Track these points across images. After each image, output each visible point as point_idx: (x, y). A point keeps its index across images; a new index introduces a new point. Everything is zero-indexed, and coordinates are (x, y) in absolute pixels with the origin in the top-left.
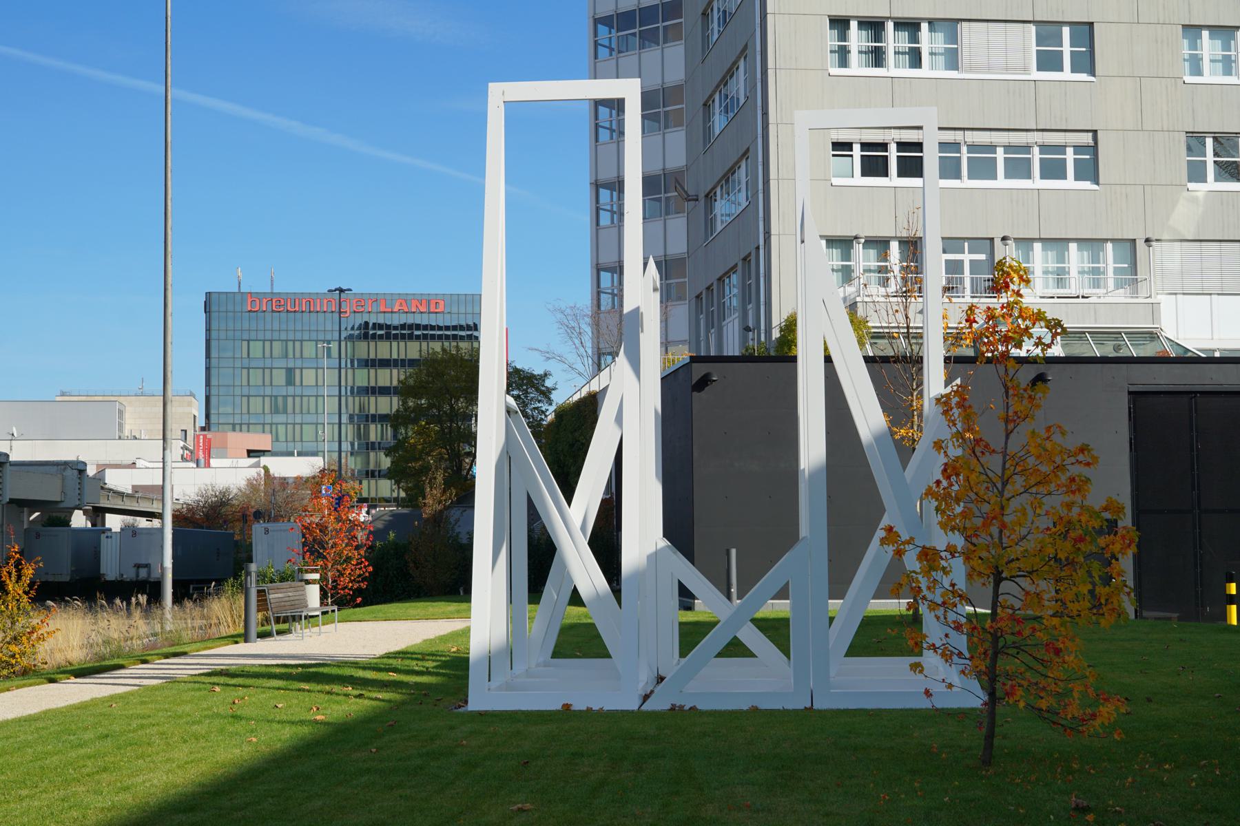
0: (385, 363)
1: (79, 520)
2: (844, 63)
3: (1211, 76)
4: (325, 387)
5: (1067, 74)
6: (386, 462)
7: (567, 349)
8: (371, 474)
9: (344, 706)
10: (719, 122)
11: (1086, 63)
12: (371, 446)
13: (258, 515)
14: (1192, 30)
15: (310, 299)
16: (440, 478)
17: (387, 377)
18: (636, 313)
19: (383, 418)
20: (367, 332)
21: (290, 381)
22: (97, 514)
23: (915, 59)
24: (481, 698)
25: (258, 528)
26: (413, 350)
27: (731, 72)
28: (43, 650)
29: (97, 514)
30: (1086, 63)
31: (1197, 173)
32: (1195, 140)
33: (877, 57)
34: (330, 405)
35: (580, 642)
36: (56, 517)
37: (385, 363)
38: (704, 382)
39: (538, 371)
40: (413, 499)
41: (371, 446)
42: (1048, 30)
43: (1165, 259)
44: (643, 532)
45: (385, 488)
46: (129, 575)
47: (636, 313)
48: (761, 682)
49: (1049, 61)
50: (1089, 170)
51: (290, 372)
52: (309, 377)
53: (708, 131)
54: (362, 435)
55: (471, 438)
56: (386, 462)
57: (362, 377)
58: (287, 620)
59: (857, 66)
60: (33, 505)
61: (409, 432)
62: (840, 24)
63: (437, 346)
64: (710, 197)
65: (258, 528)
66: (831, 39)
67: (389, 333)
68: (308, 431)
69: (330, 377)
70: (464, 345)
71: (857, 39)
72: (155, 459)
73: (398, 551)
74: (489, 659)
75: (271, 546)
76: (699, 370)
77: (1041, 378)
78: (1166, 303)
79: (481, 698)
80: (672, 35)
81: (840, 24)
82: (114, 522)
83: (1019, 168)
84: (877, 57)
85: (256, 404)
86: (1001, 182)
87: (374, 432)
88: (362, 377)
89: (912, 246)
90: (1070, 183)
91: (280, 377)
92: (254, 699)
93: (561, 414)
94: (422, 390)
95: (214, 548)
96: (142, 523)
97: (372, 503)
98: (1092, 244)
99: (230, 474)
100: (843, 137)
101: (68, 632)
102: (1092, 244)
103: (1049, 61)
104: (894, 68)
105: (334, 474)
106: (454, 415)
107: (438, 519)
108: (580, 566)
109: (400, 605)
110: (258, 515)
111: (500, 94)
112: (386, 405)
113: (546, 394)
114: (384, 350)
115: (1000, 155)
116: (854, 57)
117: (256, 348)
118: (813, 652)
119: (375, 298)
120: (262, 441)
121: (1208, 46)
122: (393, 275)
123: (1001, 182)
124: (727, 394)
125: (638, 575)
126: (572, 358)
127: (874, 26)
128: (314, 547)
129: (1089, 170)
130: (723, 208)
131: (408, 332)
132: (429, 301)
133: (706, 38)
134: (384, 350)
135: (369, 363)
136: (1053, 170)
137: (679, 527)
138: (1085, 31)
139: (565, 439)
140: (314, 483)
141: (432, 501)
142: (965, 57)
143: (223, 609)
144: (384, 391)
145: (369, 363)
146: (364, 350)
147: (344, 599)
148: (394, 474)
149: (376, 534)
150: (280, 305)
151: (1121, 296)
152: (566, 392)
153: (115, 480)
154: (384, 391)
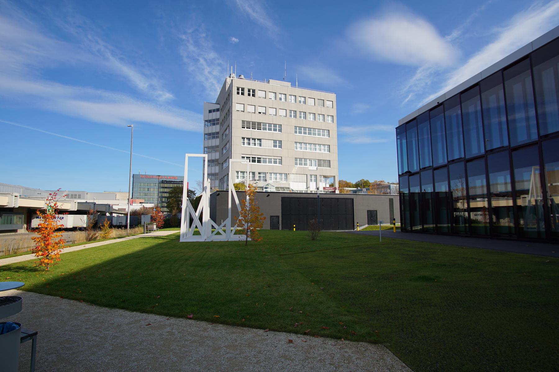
0: (166, 188)
1: (108, 214)
2: (244, 144)
3: (299, 150)
4: (155, 193)
5: (278, 148)
6: (166, 205)
7: (198, 188)
8: (163, 207)
9: (161, 241)
10: (224, 152)
11: (280, 147)
12: (163, 202)
13: (142, 214)
14: (296, 143)
15: (153, 176)
16: (176, 208)
17: (166, 190)
18: (206, 187)
19: (165, 197)
20: (163, 182)
21: (148, 190)
22: (111, 213)
23: (320, 150)
24: (182, 240)
25: (142, 216)
26: (171, 185)
27: (226, 144)
28: (111, 235)
29: (111, 213)
30: (280, 147)
31: (296, 164)
32: (296, 159)
33: (249, 144)
34: (156, 195)
35: (197, 233)
36: (103, 214)
37: (166, 188)
38: (218, 195)
39: (193, 190)
40: (171, 211)
41: (163, 202)
42: (275, 141)
43: (291, 177)
44: (206, 217)
45: (165, 209)
46: (118, 224)
47: (206, 187)
48: (222, 238)
49: (275, 146)
50: (281, 163)
51: (148, 189)
52: (152, 190)
53: (222, 153)
54: (161, 200)
55: (181, 201)
56: (166, 205)
57: (162, 190)
58: (151, 230)
59: (246, 145)
60: (98, 212)
61: (170, 200)
62: (243, 138)
63: (175, 185)
64: (222, 164)
65: (142, 216)
66: (242, 140)
67: (167, 182)
68: (151, 199)
69: (156, 190)
70: (180, 185)
71: (246, 141)
72: (122, 204)
73: (168, 220)
74: (183, 235)
75: (145, 219)
76: (218, 193)
77: (268, 195)
78: (291, 183)
79: (182, 240)
80: (217, 137)
81: (243, 138)
82: (114, 215)
83: (270, 162)
84: (249, 144)
85: (142, 194)
86: (267, 164)
87: (164, 199)
88: (162, 190)
89: (254, 173)
90: (278, 164)
91: (146, 189)
92: (148, 241)
93: (196, 198)
94: (172, 193)
95: (136, 220)
96: (120, 215)
97: (163, 212)
98: (281, 174)
99: (136, 207)
100: (243, 156)
101: (114, 232)
102: (281, 174)
103: (275, 146)
104: (252, 146)
105: (157, 207)
106: (178, 197)
107: (175, 215)
108: (196, 222)
109: (98, 262)
110: (142, 214)
111: (187, 155)
112: (166, 195)
113: (195, 194)
114: (166, 185)
115: (267, 160)
116: (245, 144)
117: (142, 184)
118: (229, 233)
119: (165, 176)
120: (143, 201)
121: (298, 145)
122: (168, 171)
123: (267, 164)
124: (218, 199)
125: (205, 222)
126: (199, 189)
127: (249, 139)
128: (153, 219)
129: (281, 163)
130: (224, 165)
131: (170, 182)
132: (174, 177)
133: (223, 138)
134: (166, 185)
135: (163, 188)
136: (275, 162)
137: (213, 216)
138: (280, 142)
139: (195, 203)
140: (153, 208)
141: (174, 212)
142: (262, 144)
143: (138, 229)
144: (166, 192)
145: (163, 188)
146: (162, 185)
147: (160, 228)
148: (167, 207)
149: (166, 217)
150: (147, 177)
151: (285, 182)
152: (198, 195)
153: (114, 207)
154: (166, 192)
